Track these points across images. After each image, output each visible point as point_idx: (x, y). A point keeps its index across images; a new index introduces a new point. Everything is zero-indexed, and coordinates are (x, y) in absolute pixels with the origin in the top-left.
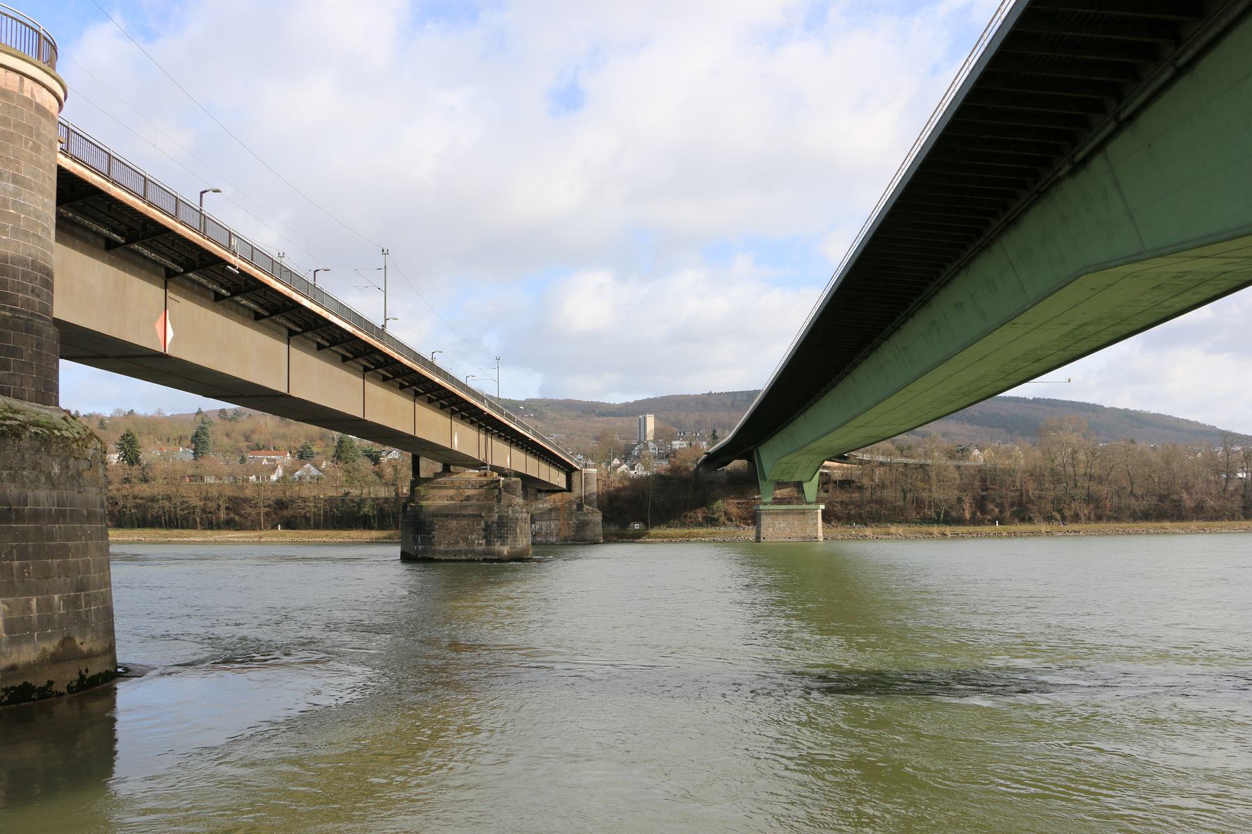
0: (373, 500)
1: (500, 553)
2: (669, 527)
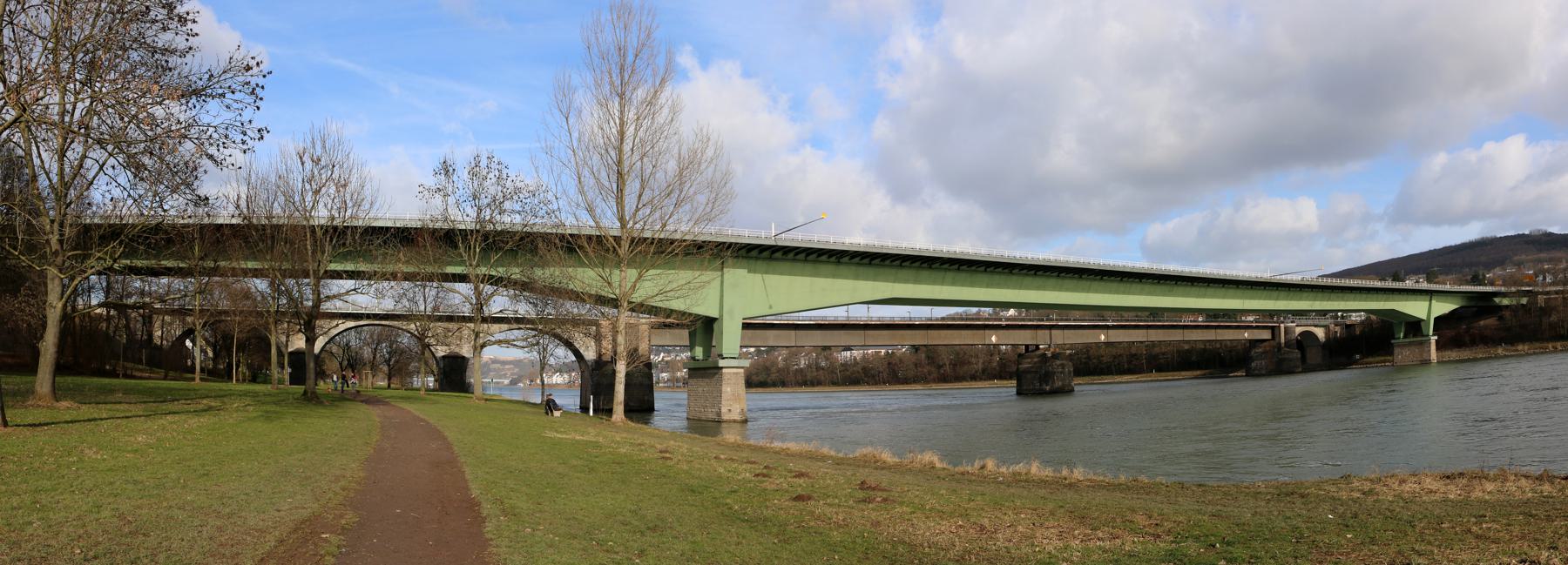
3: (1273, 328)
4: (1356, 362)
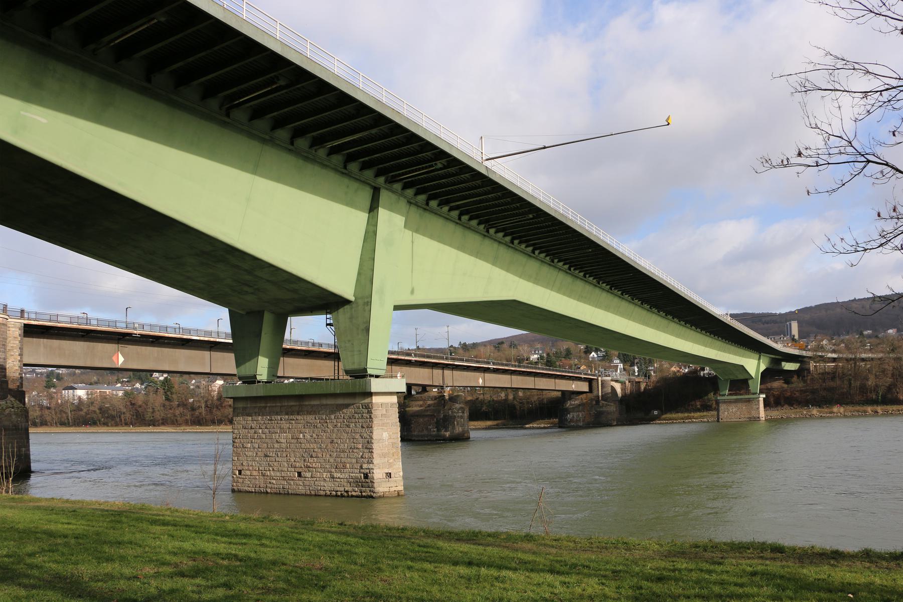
2: (678, 412)
3: (590, 381)
4: (657, 418)
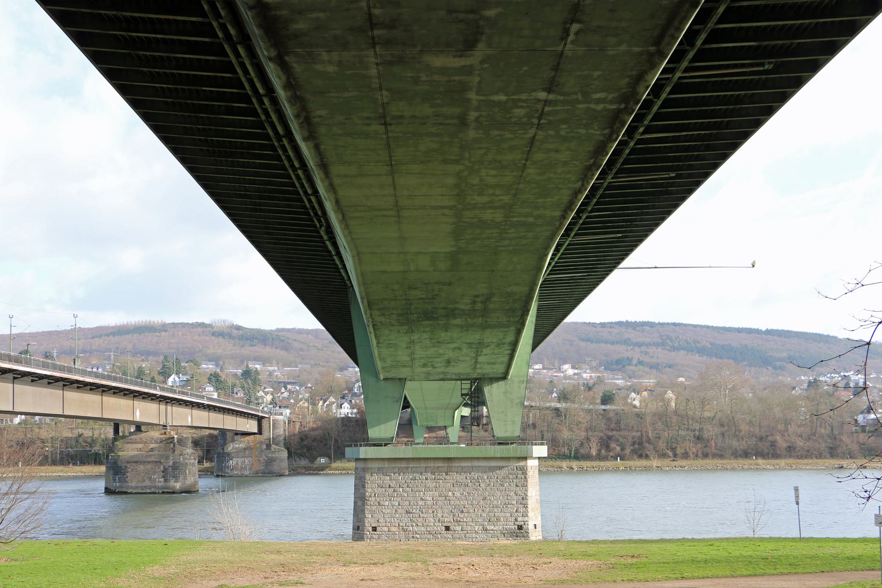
0: (103, 440)
1: (174, 487)
3: (260, 419)
